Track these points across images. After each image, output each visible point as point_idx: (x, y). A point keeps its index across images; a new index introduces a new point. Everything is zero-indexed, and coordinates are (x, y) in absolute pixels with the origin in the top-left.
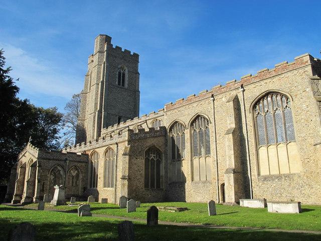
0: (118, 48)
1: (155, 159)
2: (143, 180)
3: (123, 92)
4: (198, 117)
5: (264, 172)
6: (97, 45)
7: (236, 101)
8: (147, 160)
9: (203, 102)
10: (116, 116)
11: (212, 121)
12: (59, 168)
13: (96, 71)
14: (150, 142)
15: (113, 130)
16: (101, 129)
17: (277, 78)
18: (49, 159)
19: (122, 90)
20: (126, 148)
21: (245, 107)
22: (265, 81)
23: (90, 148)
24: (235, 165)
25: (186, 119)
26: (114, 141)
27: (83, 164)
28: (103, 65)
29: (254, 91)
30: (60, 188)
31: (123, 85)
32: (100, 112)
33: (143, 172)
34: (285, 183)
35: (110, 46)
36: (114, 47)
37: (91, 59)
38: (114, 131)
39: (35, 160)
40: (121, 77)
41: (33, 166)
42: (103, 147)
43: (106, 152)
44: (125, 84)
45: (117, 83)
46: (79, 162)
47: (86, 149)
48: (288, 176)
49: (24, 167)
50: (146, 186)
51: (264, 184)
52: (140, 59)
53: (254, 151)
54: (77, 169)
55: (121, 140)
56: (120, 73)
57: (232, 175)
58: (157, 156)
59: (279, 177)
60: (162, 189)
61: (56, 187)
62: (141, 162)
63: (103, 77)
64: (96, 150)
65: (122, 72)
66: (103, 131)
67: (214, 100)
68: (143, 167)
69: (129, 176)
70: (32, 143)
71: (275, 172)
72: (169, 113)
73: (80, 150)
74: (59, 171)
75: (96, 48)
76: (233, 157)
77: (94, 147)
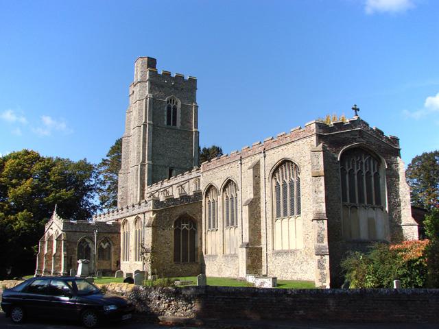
0: (166, 74)
1: (188, 229)
2: (172, 253)
3: (174, 135)
4: (285, 162)
5: (278, 247)
6: (139, 71)
7: (256, 167)
8: (177, 232)
9: (233, 165)
10: (166, 167)
11: (240, 188)
12: (88, 241)
13: (137, 108)
14: (179, 212)
15: (157, 188)
16: (144, 187)
17: (291, 145)
18: (76, 232)
19: (174, 131)
20: (151, 218)
21: (265, 172)
22: (283, 147)
23: (121, 216)
24: (250, 239)
25: (219, 184)
26: (141, 210)
27: (115, 235)
28: (144, 100)
29: (274, 157)
30: (82, 262)
31: (175, 123)
32: (143, 165)
33: (172, 245)
34: (290, 258)
35: (154, 74)
36: (160, 72)
37: (132, 88)
38: (157, 191)
39: (60, 232)
40: (172, 113)
41: (58, 239)
42: (132, 216)
43: (136, 221)
44: (177, 122)
45: (165, 123)
46: (109, 233)
47: (118, 217)
48: (293, 252)
49: (50, 240)
50: (176, 259)
51: (276, 259)
52: (199, 85)
53: (271, 225)
54: (108, 241)
55: (146, 209)
56: (169, 108)
57: (245, 249)
58: (190, 224)
59: (286, 252)
60: (197, 263)
61: (395, 287)
62: (170, 233)
63: (146, 118)
64: (127, 219)
65: (172, 106)
66: (148, 190)
67: (265, 157)
68: (172, 239)
69: (153, 248)
70: (59, 213)
71: (286, 248)
72: (205, 174)
73: (110, 218)
74: (87, 243)
75: (138, 77)
76: (248, 229)
77: (125, 215)
